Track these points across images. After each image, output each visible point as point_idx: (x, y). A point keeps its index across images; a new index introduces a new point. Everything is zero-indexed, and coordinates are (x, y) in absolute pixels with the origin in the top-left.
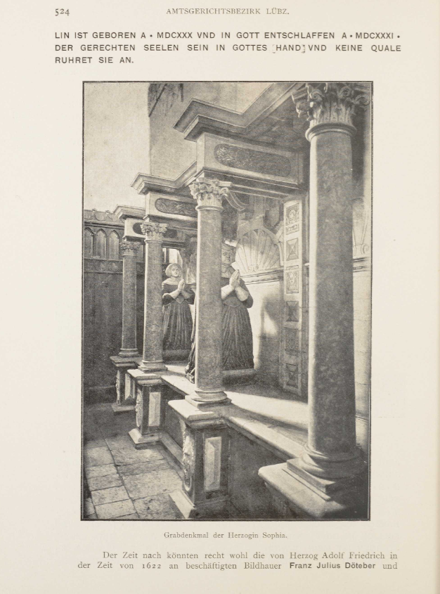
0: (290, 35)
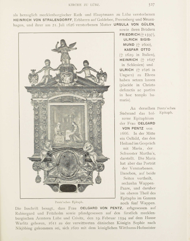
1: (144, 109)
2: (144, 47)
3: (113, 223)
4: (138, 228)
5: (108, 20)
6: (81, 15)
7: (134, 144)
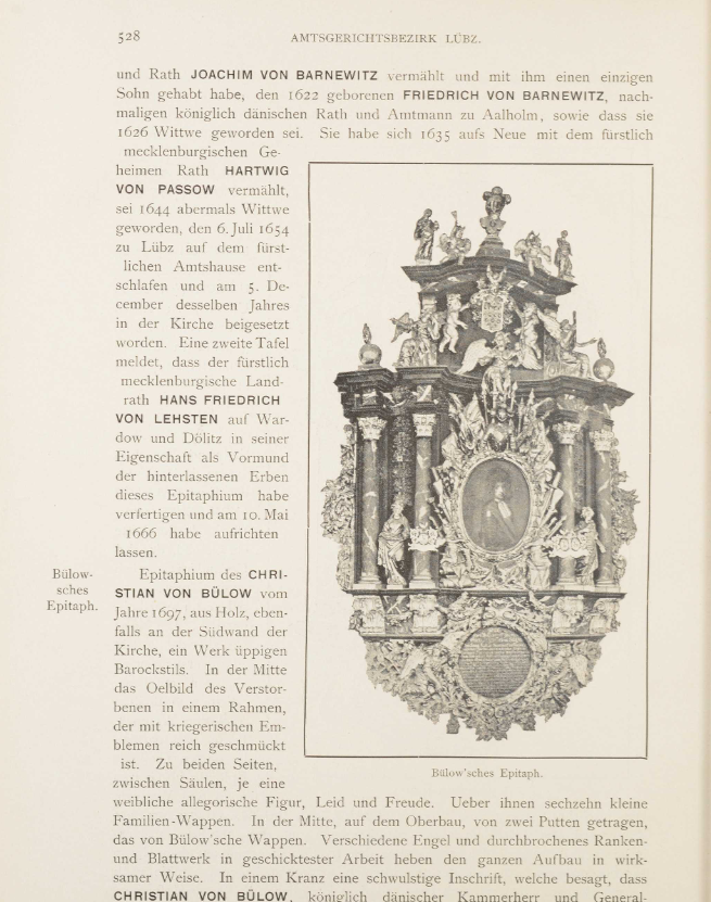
0: (465, 95)
1: (257, 691)
4: (221, 615)
6: (175, 74)
7: (215, 516)
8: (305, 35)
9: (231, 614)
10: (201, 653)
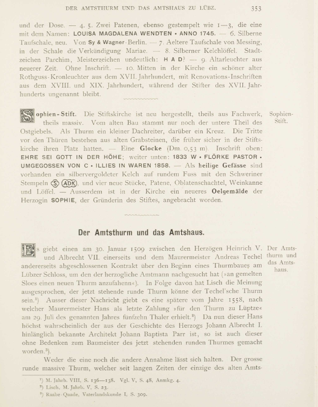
2: (146, 30)
3: (154, 68)
5: (41, 132)
8: (88, 7)
9: (124, 335)
10: (233, 184)
